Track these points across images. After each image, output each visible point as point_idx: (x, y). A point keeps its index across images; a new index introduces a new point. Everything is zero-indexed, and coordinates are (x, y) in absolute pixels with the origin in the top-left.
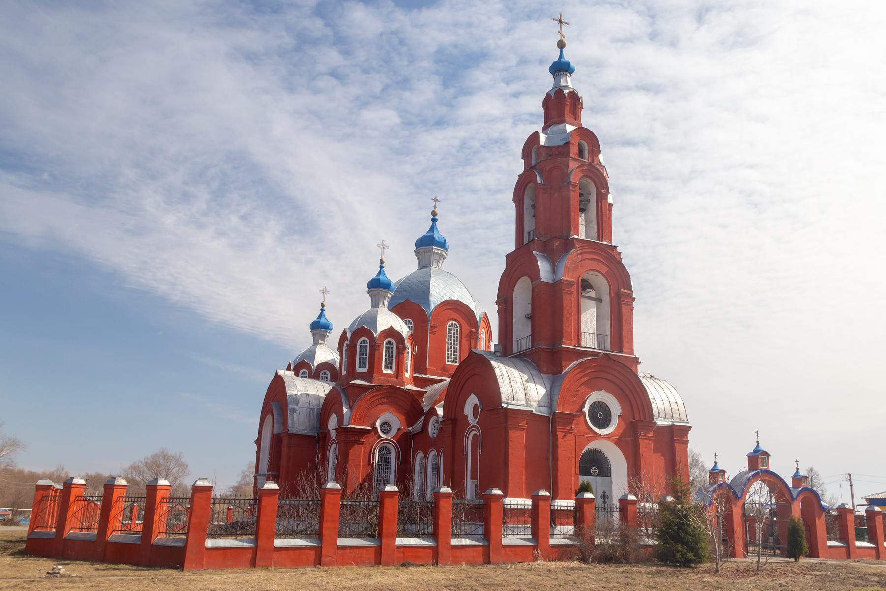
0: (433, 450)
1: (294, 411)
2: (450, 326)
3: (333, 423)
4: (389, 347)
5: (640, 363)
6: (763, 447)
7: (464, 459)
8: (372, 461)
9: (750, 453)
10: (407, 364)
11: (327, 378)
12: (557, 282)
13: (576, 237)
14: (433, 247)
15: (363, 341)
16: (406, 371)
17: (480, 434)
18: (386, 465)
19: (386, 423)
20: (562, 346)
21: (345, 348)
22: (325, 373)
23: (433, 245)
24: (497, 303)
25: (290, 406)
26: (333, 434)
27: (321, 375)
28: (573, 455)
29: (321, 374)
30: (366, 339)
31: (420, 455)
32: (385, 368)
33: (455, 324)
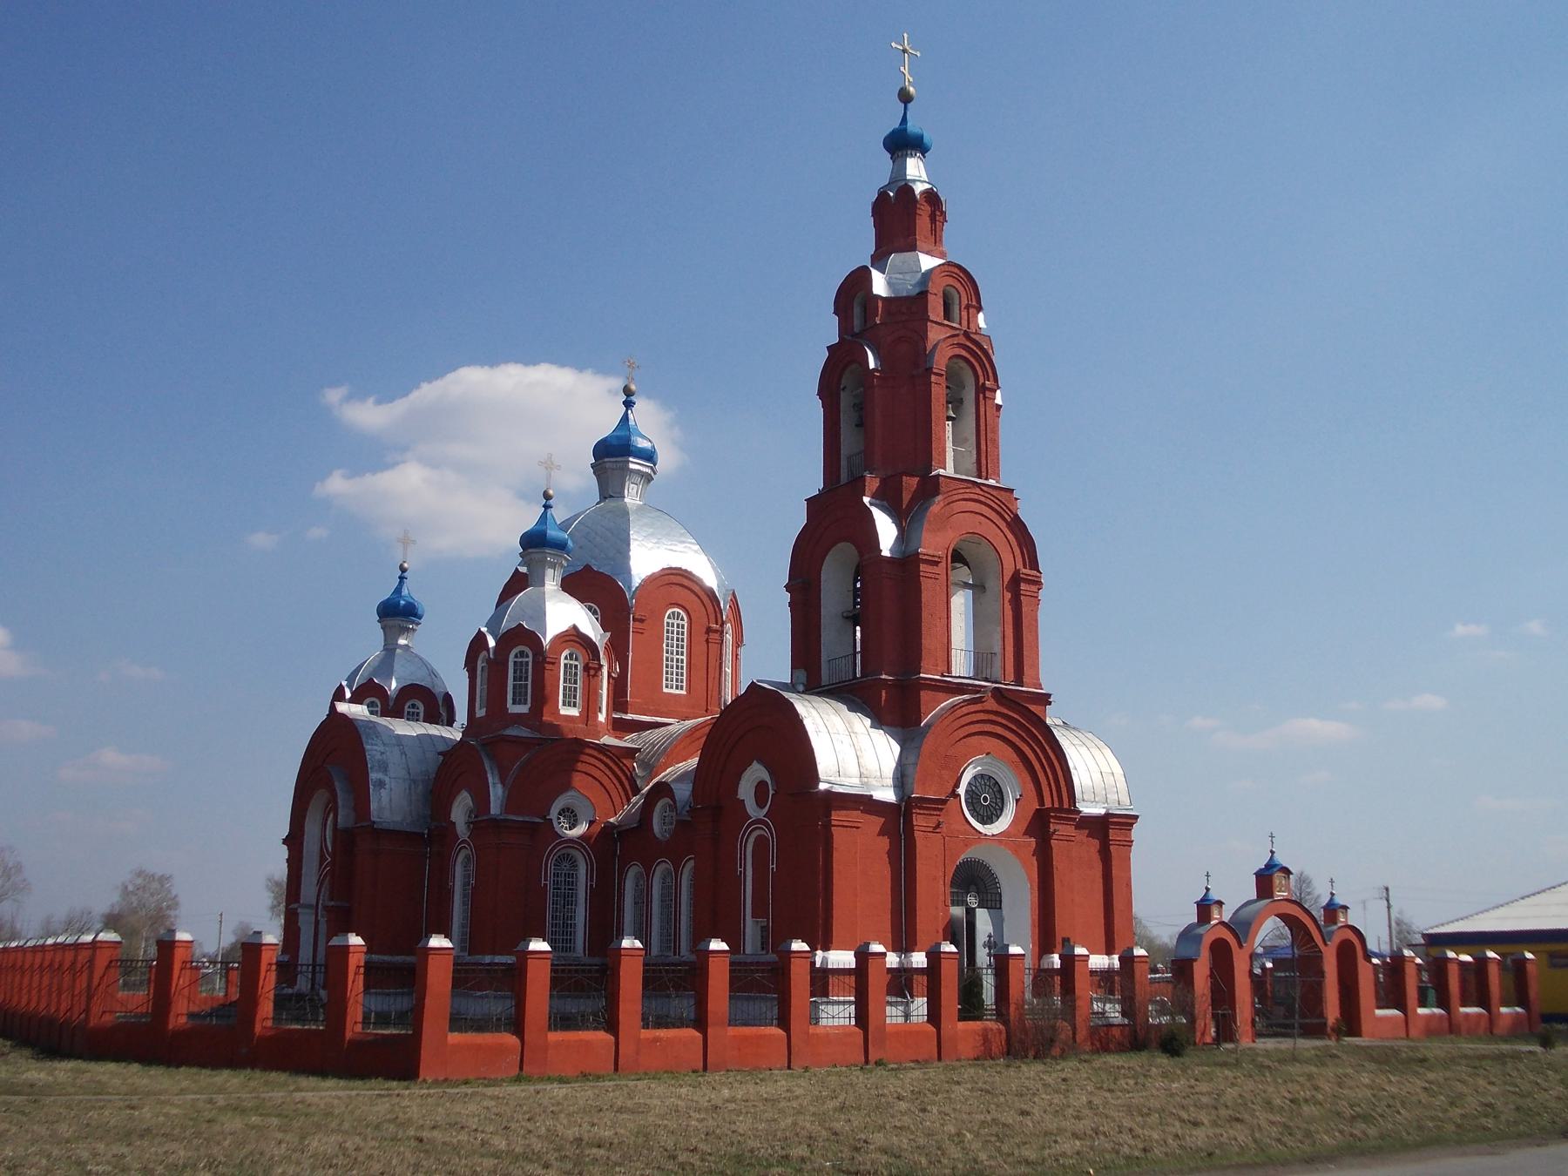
0: (665, 862)
1: (381, 784)
2: (669, 617)
3: (460, 810)
4: (571, 665)
5: (1050, 703)
6: (1281, 859)
7: (738, 881)
8: (543, 882)
9: (1261, 870)
10: (602, 694)
11: (418, 714)
12: (908, 557)
13: (941, 471)
14: (631, 459)
15: (520, 652)
16: (600, 711)
17: (772, 834)
18: (569, 889)
19: (568, 809)
20: (921, 675)
21: (480, 665)
22: (413, 706)
23: (630, 456)
24: (788, 588)
25: (373, 776)
26: (462, 829)
27: (406, 709)
28: (941, 874)
29: (406, 707)
30: (527, 650)
31: (633, 872)
32: (564, 704)
33: (679, 614)
